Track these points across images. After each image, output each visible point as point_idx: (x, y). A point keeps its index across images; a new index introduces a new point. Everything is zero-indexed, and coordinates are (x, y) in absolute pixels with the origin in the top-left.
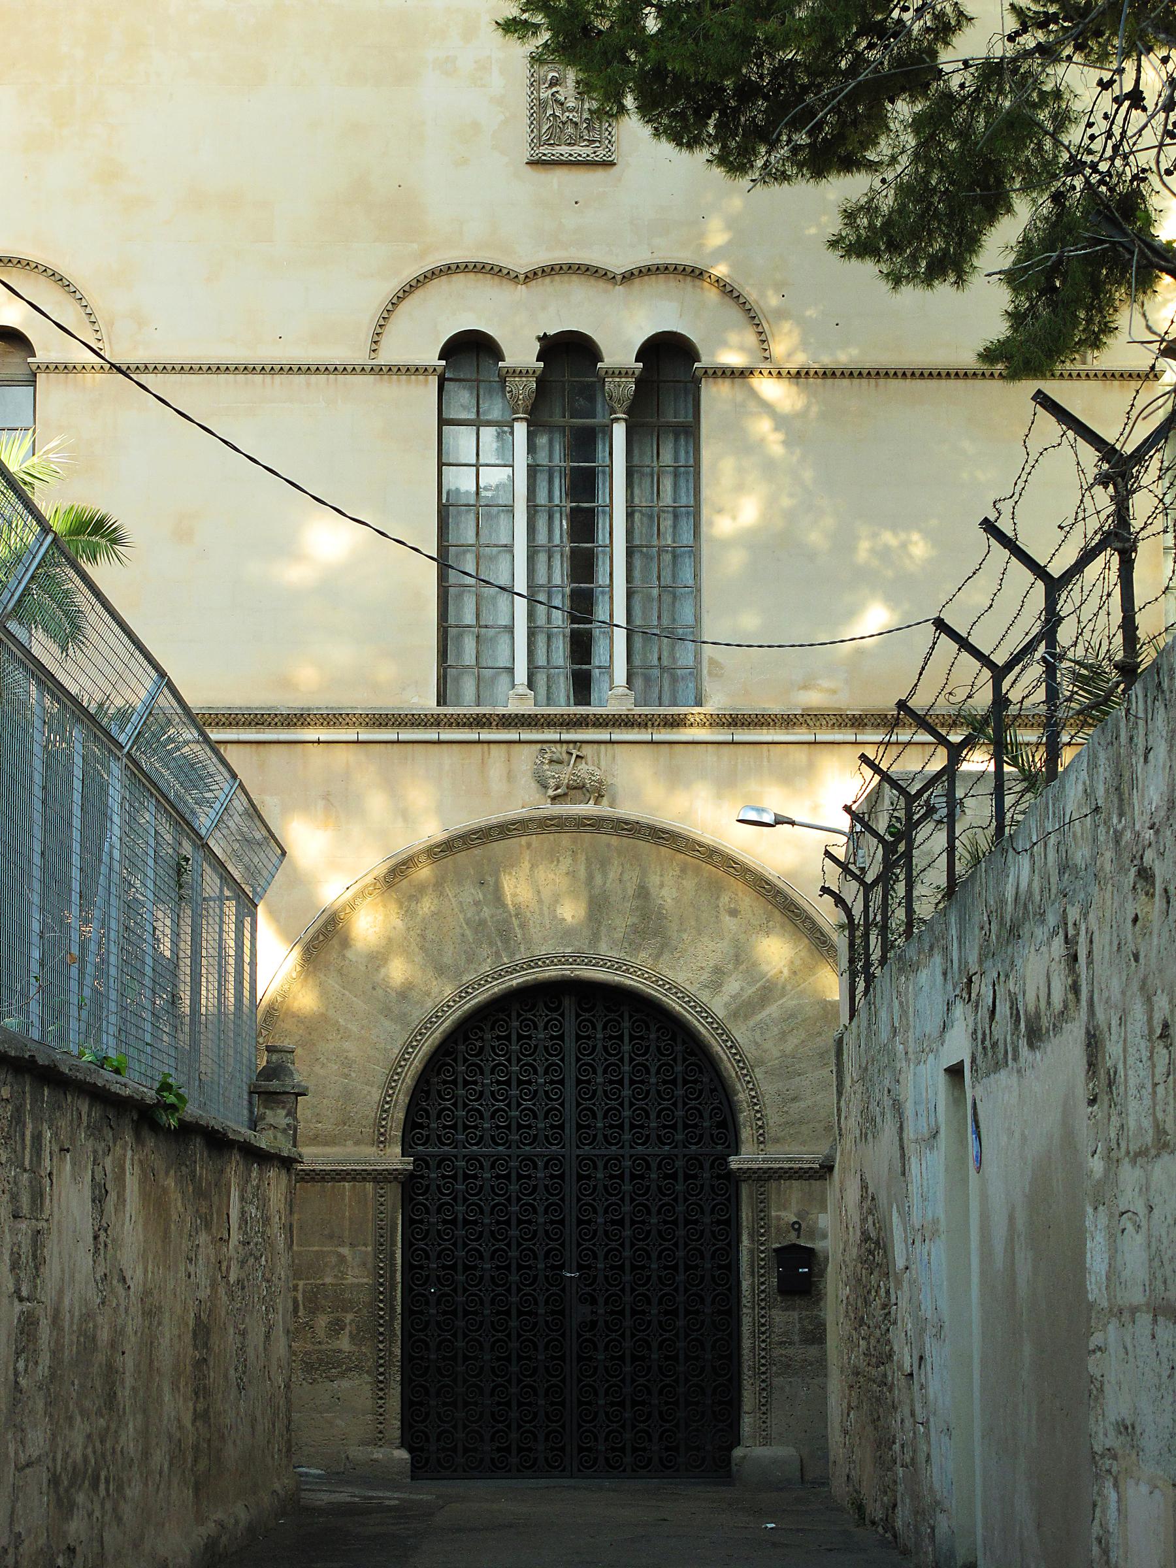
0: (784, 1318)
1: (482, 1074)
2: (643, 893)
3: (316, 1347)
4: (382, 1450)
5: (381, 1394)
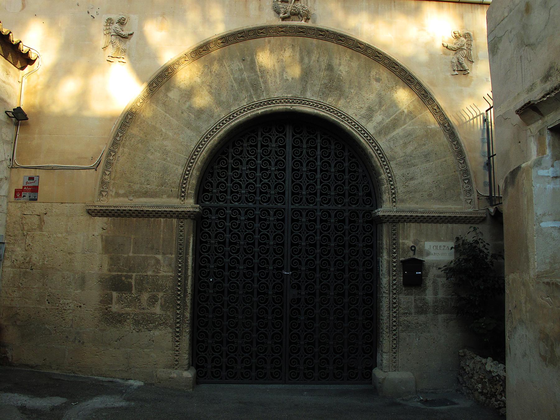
0: (407, 300)
1: (241, 164)
2: (330, 68)
3: (141, 311)
4: (177, 371)
5: (177, 339)
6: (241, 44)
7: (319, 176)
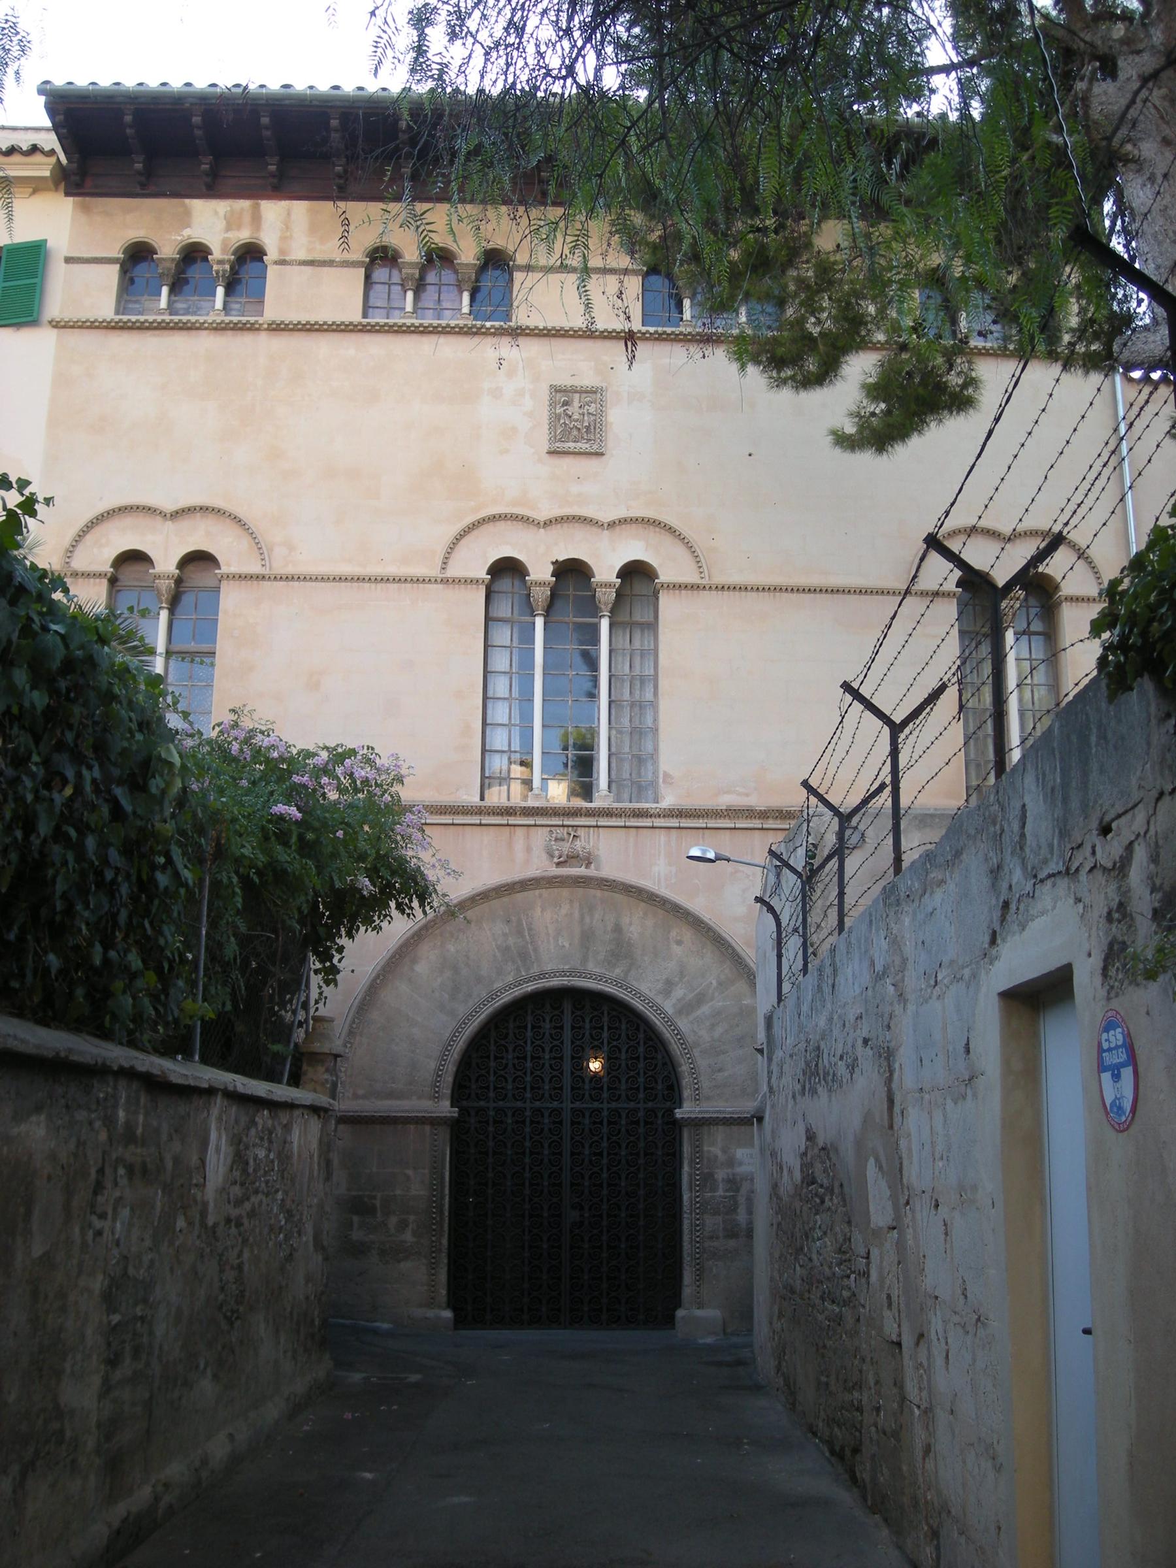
2: (618, 929)
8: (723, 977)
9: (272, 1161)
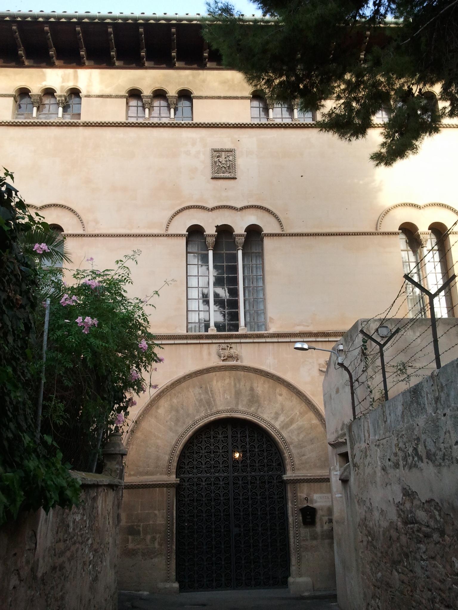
0: (304, 531)
2: (252, 389)
6: (199, 377)
7: (248, 440)
8: (302, 410)
9: (85, 521)
